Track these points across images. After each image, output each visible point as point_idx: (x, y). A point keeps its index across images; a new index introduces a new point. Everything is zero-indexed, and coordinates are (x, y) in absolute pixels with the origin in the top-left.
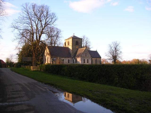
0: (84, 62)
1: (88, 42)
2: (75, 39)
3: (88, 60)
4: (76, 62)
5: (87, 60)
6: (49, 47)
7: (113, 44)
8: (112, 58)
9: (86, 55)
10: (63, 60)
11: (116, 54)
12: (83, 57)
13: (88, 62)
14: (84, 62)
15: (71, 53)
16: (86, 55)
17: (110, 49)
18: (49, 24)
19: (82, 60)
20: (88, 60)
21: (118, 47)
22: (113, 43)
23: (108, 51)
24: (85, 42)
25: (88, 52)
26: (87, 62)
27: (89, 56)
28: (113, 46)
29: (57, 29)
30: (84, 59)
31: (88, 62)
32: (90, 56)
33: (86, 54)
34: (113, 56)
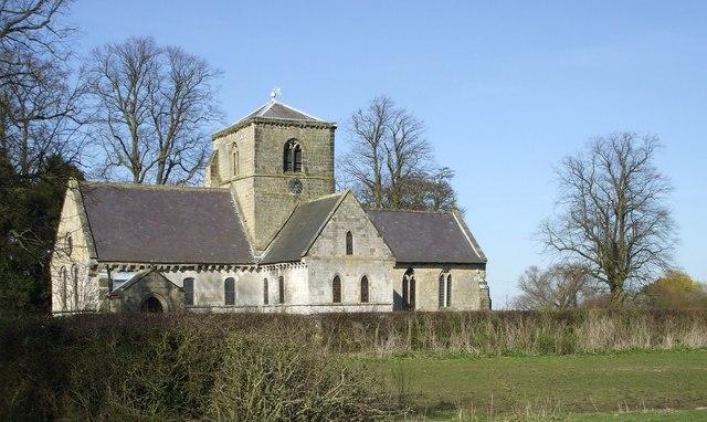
0: (337, 296)
1: (407, 148)
2: (277, 129)
3: (364, 281)
4: (282, 301)
5: (358, 279)
6: (87, 195)
7: (600, 159)
8: (595, 266)
9: (349, 250)
10: (189, 282)
11: (622, 233)
12: (328, 261)
13: (364, 297)
14: (337, 296)
15: (252, 233)
16: (349, 250)
17: (576, 191)
18: (18, 29)
19: (321, 283)
20: (364, 281)
21: (637, 181)
22: (598, 150)
23: (564, 209)
24: (390, 145)
25: (371, 227)
26: (356, 297)
27: (377, 254)
28: (600, 170)
29: (175, 55)
30: (332, 276)
31: (364, 297)
32: (380, 248)
33: (349, 235)
34: (600, 247)
